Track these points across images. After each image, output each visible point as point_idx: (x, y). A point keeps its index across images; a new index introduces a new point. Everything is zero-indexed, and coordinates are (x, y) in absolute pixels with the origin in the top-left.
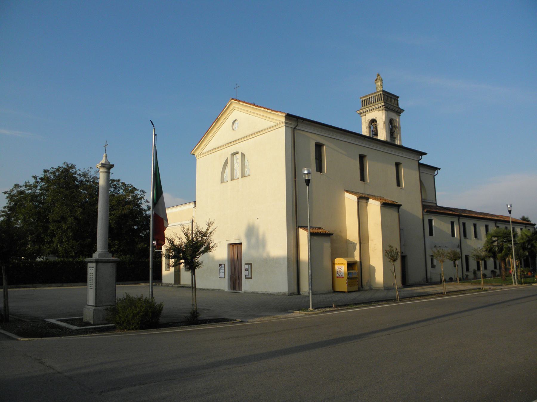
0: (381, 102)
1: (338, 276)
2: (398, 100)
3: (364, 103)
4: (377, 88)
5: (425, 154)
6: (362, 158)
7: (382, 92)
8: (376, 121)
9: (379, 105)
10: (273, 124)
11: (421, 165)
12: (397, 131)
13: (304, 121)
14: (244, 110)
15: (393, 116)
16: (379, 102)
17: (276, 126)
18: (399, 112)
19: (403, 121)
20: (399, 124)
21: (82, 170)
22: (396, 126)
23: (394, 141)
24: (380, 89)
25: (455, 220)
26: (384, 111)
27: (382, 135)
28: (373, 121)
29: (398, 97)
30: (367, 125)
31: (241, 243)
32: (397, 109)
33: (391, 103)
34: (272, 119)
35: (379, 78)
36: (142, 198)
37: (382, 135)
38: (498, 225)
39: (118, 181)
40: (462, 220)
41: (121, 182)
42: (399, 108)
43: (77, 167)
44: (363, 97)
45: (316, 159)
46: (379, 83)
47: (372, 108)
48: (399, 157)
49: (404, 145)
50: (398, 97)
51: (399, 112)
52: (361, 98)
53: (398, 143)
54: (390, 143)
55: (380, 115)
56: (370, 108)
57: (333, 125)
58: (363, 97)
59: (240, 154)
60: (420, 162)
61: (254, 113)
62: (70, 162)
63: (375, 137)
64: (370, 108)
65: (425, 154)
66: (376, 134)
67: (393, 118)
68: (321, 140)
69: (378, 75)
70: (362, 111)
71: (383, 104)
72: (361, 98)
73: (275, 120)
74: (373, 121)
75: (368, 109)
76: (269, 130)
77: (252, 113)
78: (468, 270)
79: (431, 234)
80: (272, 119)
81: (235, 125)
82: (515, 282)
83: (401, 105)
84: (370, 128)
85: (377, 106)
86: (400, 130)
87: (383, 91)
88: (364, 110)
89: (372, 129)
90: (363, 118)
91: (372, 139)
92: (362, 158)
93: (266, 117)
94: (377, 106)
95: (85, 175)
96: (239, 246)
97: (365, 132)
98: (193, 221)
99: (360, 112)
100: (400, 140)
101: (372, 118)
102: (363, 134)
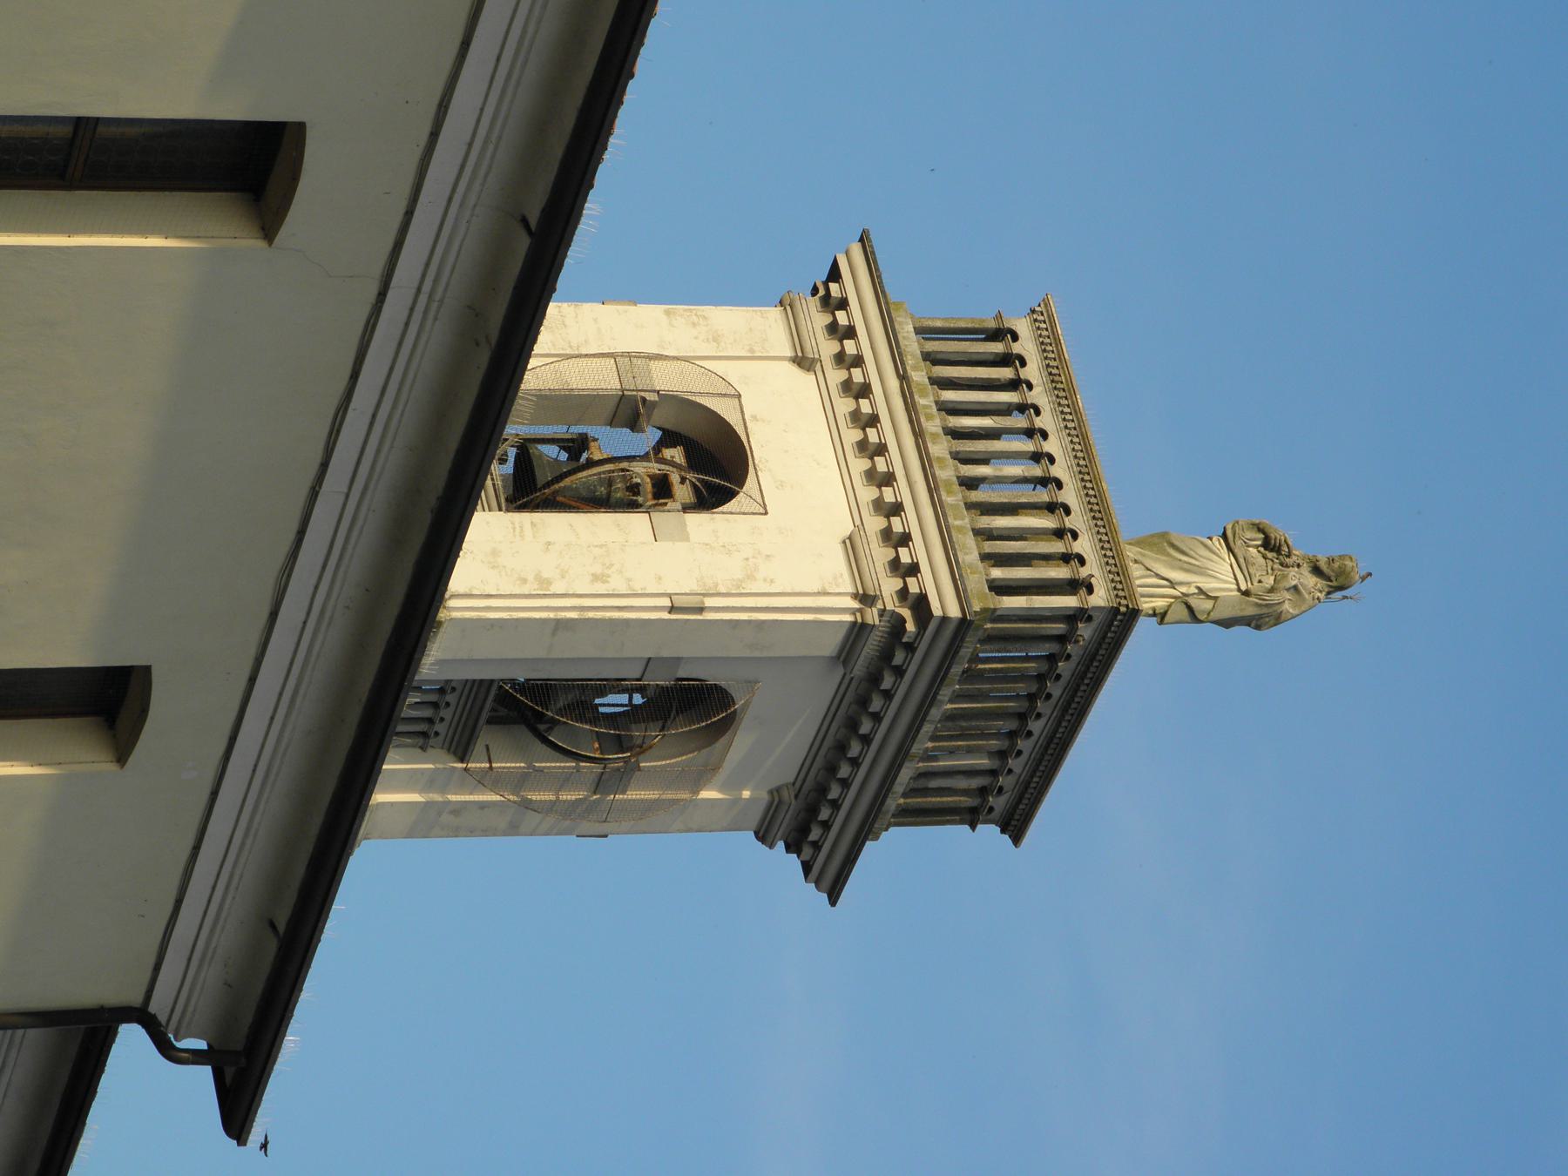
0: (976, 582)
2: (972, 817)
3: (976, 367)
4: (1161, 542)
5: (237, 1111)
6: (245, 166)
7: (1100, 598)
8: (711, 497)
9: (926, 551)
11: (81, 1042)
12: (558, 779)
15: (771, 744)
16: (970, 552)
18: (817, 827)
19: (690, 870)
20: (645, 817)
22: (622, 779)
23: (423, 739)
24: (1146, 605)
26: (840, 606)
27: (519, 571)
28: (711, 463)
29: (1015, 826)
30: (666, 379)
32: (844, 821)
33: (949, 718)
35: (1301, 577)
37: (519, 571)
42: (867, 831)
44: (1050, 343)
45: (82, 126)
46: (1220, 577)
47: (902, 456)
48: (223, 733)
49: (365, 866)
50: (1015, 826)
51: (817, 827)
52: (1043, 318)
53: (403, 782)
54: (390, 687)
55: (788, 553)
56: (894, 431)
57: (635, 92)
58: (1050, 343)
60: (131, 1040)
63: (500, 472)
64: (894, 431)
65: (237, 1111)
66: (528, 492)
67: (742, 742)
68: (177, 722)
69: (1335, 579)
70: (862, 312)
71: (945, 604)
72: (1043, 318)
74: (711, 463)
75: (886, 397)
83: (906, 862)
84: (628, 410)
85: (919, 519)
86: (568, 819)
87: (1120, 621)
88: (870, 341)
89: (610, 441)
90: (769, 326)
91: (481, 436)
92: (245, 166)
94: (919, 519)
97: (584, 340)
99: (856, 286)
100: (425, 823)
101: (763, 446)
102: (555, 310)
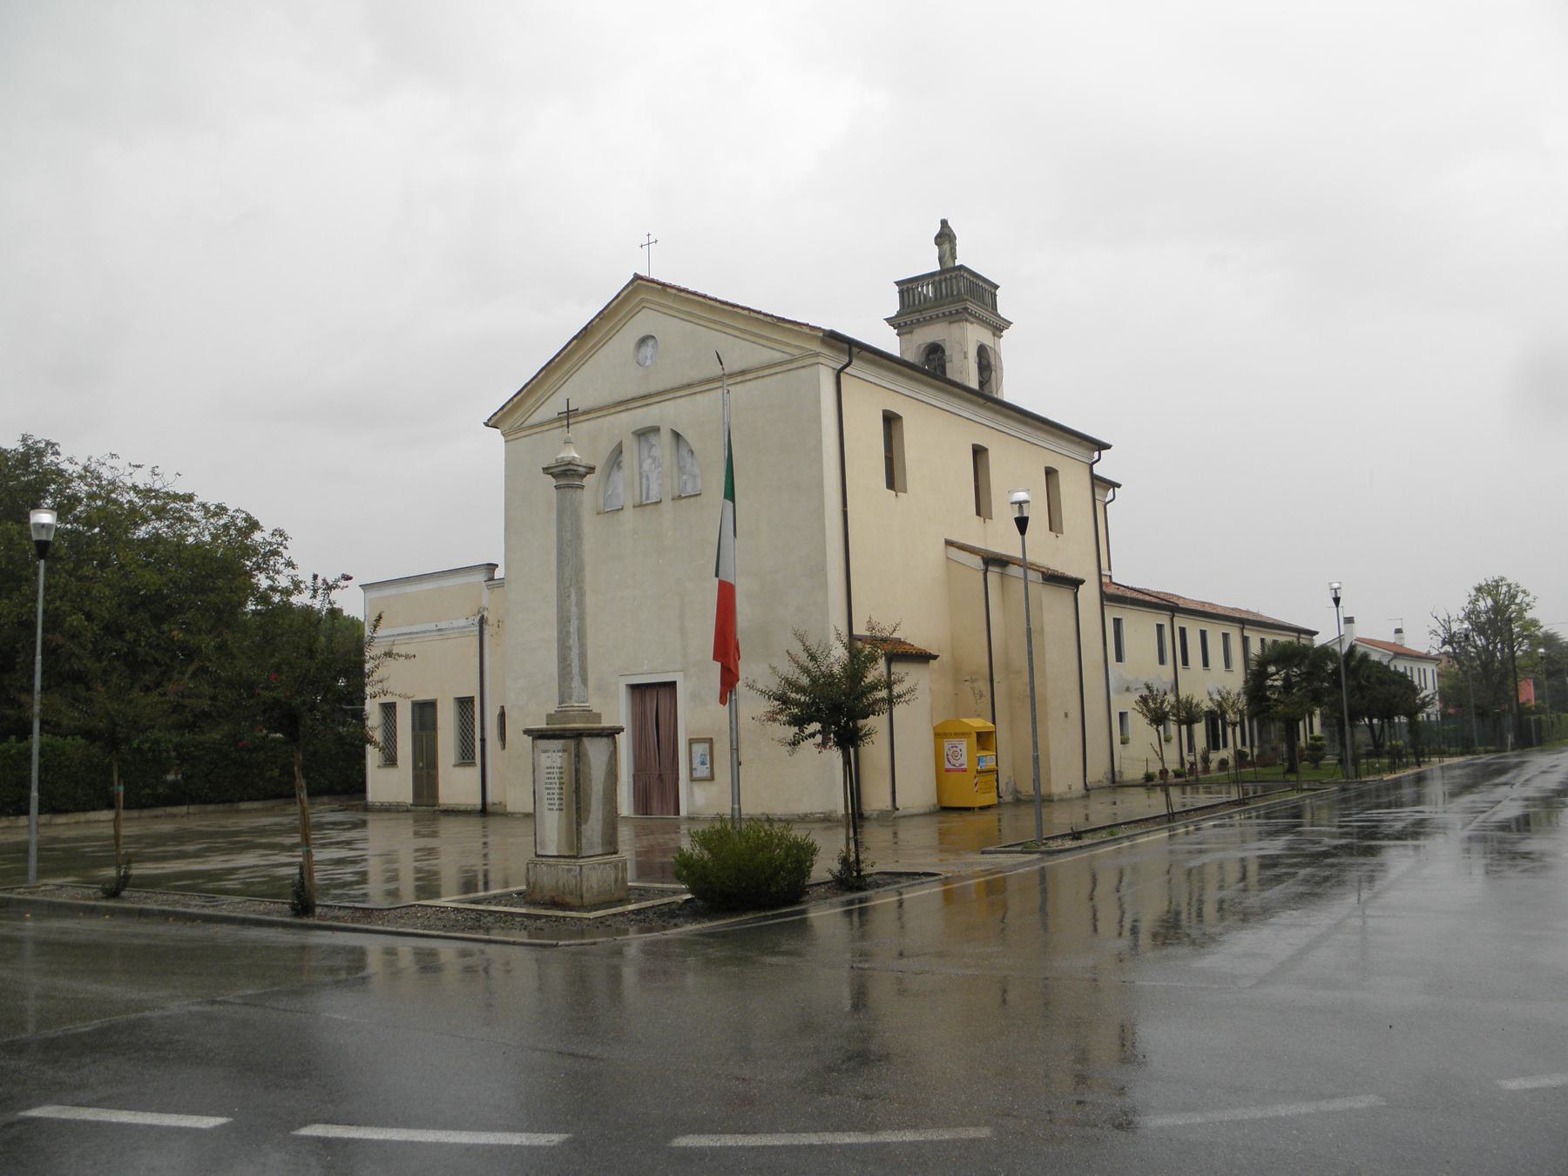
1: (948, 766)
8: (943, 351)
10: (778, 356)
13: (864, 353)
14: (678, 310)
17: (791, 361)
21: (83, 461)
25: (1164, 619)
29: (997, 287)
31: (673, 685)
34: (776, 341)
36: (275, 553)
38: (1246, 633)
39: (189, 498)
40: (1180, 621)
41: (197, 500)
43: (65, 452)
50: (997, 287)
59: (666, 436)
61: (715, 322)
62: (40, 435)
73: (788, 345)
76: (767, 372)
77: (710, 320)
78: (1191, 747)
79: (1119, 658)
80: (776, 341)
81: (648, 350)
82: (348, 843)
93: (757, 335)
95: (88, 473)
96: (664, 695)
98: (482, 621)
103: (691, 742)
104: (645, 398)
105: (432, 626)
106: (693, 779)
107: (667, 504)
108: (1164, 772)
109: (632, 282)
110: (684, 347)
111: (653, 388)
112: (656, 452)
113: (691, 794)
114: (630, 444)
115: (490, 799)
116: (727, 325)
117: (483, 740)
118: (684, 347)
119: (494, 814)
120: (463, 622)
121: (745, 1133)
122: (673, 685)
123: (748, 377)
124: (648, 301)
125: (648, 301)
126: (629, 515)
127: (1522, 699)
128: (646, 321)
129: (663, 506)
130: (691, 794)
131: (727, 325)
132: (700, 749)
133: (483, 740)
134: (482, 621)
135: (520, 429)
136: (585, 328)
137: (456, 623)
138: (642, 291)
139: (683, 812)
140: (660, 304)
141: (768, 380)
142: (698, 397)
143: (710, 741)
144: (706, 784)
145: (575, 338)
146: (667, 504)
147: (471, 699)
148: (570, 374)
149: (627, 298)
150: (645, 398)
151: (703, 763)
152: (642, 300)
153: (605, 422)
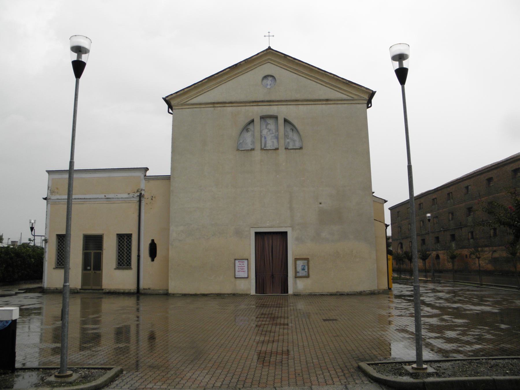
10: (349, 98)
17: (353, 100)
61: (311, 76)
81: (269, 81)
98: (141, 196)
103: (296, 260)
104: (270, 102)
105: (102, 196)
106: (296, 277)
107: (282, 150)
108: (276, 325)
109: (267, 50)
110: (289, 83)
111: (273, 98)
112: (269, 127)
113: (295, 283)
114: (257, 120)
115: (142, 286)
116: (317, 79)
117: (139, 256)
118: (289, 83)
119: (145, 294)
120: (126, 196)
121: (516, 375)
122: (285, 233)
123: (329, 102)
124: (271, 60)
125: (271, 60)
126: (257, 155)
127: (68, 371)
128: (268, 69)
129: (279, 151)
130: (295, 283)
131: (317, 79)
132: (300, 263)
133: (139, 256)
134: (141, 196)
135: (184, 104)
136: (236, 65)
137: (119, 196)
138: (270, 54)
139: (291, 291)
140: (279, 63)
141: (340, 106)
142: (300, 106)
143: (307, 259)
144: (305, 279)
145: (229, 68)
146: (282, 150)
147: (129, 236)
148: (220, 84)
149: (261, 56)
150: (270, 102)
151: (303, 269)
152: (269, 59)
153: (243, 109)
